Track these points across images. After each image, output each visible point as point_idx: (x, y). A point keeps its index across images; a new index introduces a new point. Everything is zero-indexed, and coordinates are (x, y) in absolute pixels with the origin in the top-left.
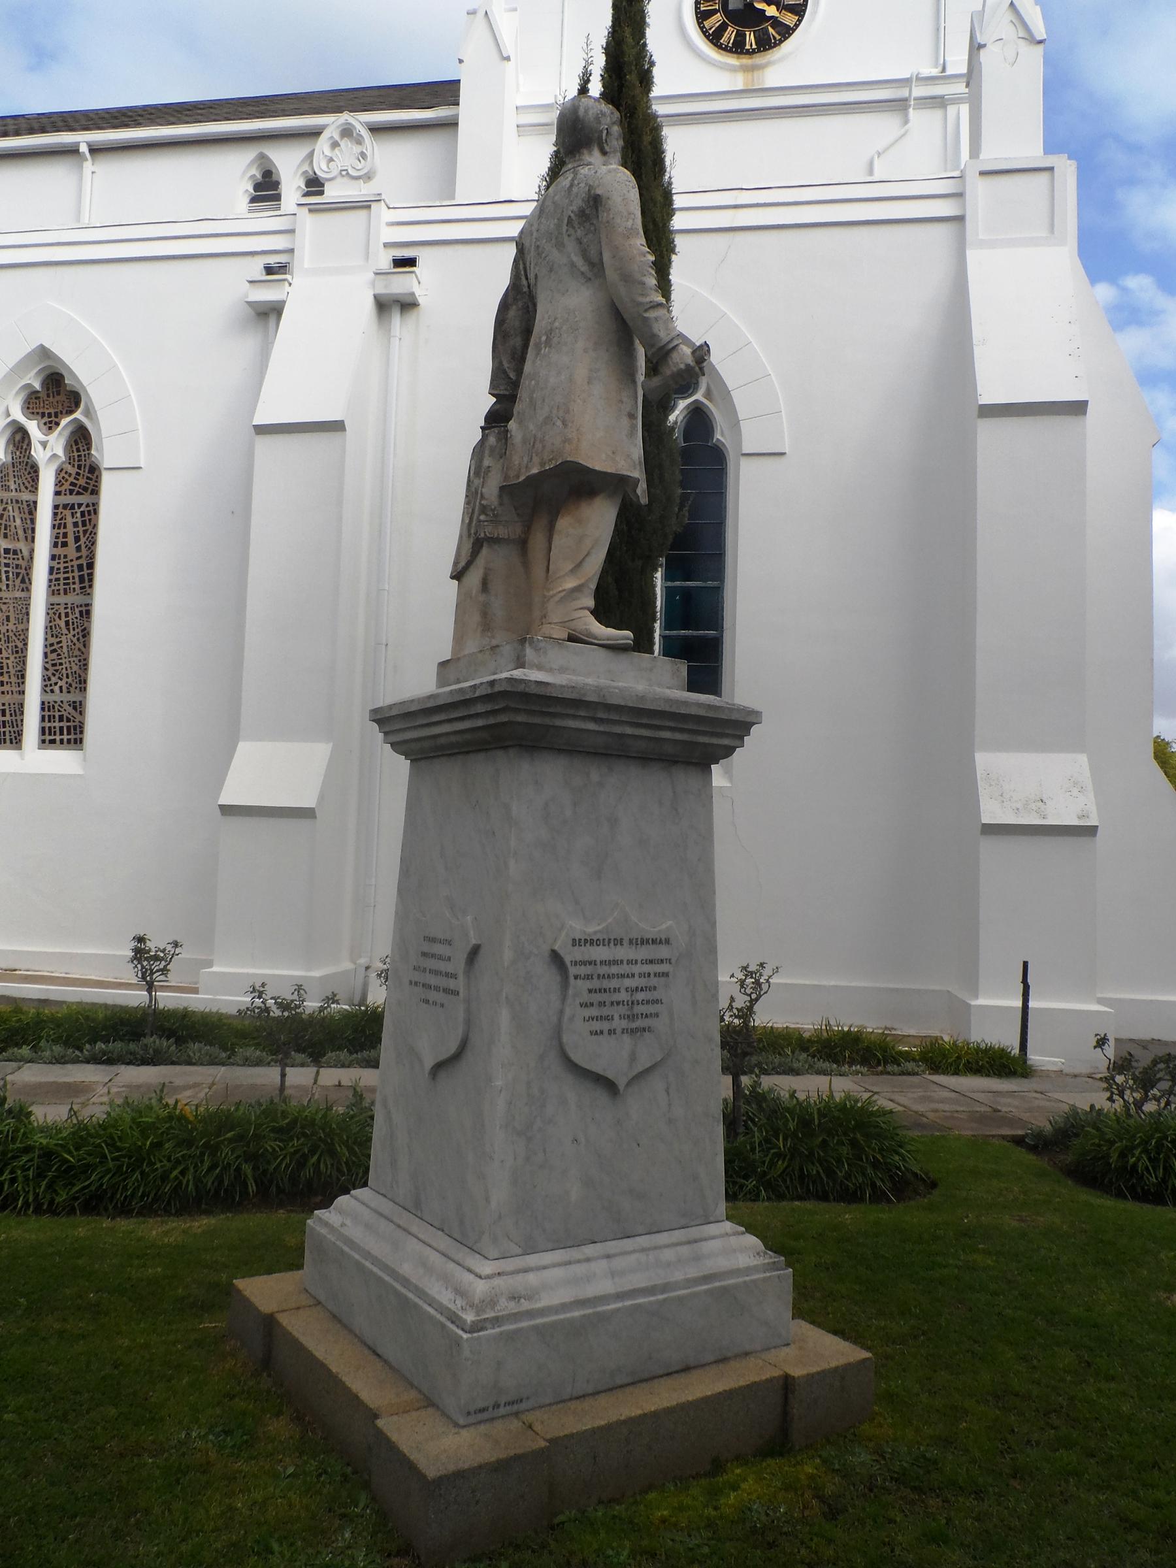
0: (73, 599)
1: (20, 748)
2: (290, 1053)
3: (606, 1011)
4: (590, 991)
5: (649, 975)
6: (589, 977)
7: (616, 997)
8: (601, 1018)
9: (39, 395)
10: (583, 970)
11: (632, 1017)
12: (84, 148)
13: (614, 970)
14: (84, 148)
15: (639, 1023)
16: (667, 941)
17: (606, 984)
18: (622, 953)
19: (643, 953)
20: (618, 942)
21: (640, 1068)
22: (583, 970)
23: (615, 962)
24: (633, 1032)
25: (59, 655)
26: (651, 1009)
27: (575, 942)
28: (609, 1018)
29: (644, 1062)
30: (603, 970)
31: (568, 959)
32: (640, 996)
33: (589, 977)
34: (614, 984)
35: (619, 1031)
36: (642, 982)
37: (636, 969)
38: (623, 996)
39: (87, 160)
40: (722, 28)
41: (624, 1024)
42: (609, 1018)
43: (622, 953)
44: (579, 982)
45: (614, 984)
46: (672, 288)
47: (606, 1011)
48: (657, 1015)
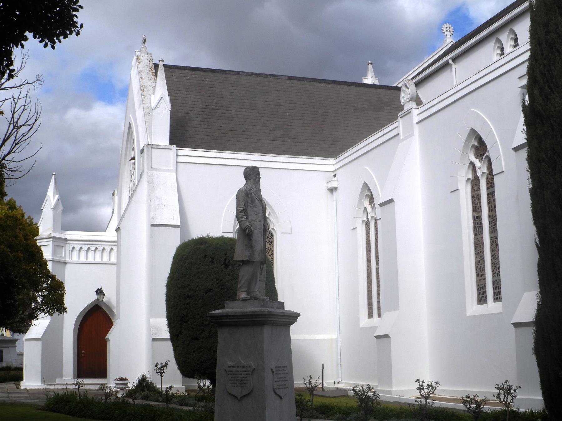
0: (478, 237)
1: (486, 303)
2: (145, 385)
3: (236, 382)
4: (232, 377)
5: (245, 374)
6: (231, 374)
7: (238, 379)
8: (234, 383)
9: (478, 148)
10: (230, 373)
11: (241, 383)
12: (450, 61)
13: (237, 373)
14: (450, 61)
15: (243, 385)
16: (250, 367)
17: (235, 376)
18: (239, 369)
19: (244, 369)
20: (238, 367)
21: (243, 395)
22: (230, 373)
23: (237, 371)
24: (241, 387)
25: (495, 260)
26: (245, 382)
27: (229, 367)
28: (236, 383)
29: (244, 393)
30: (234, 373)
31: (227, 370)
32: (243, 379)
33: (231, 374)
34: (237, 376)
35: (238, 386)
36: (244, 376)
37: (242, 373)
38: (239, 379)
39: (452, 65)
40: (36, 305)
41: (239, 385)
42: (236, 383)
43: (239, 369)
44: (229, 375)
45: (237, 376)
46: (525, 82)
47: (236, 382)
48: (247, 383)
